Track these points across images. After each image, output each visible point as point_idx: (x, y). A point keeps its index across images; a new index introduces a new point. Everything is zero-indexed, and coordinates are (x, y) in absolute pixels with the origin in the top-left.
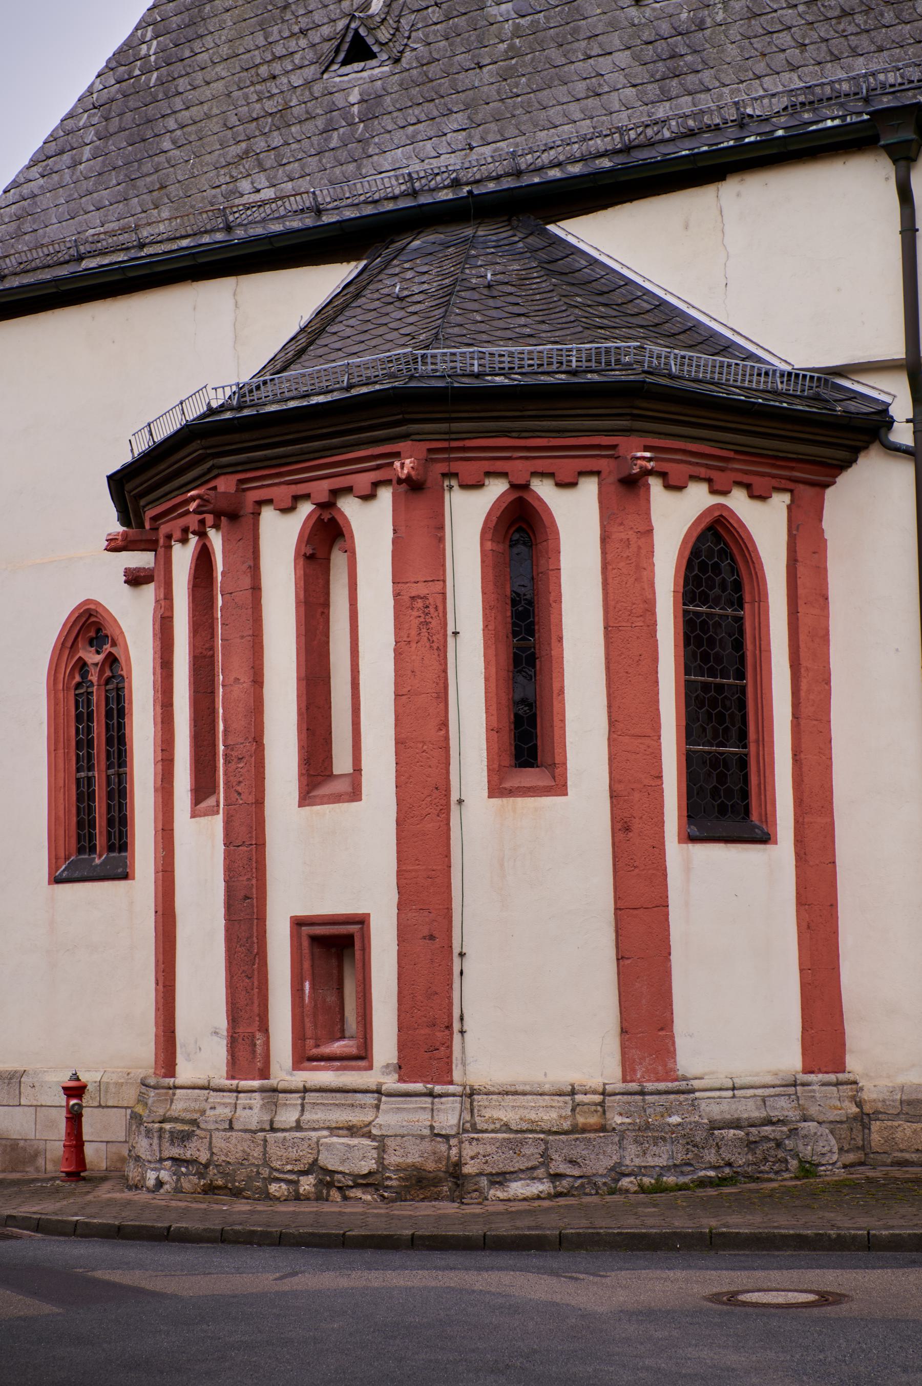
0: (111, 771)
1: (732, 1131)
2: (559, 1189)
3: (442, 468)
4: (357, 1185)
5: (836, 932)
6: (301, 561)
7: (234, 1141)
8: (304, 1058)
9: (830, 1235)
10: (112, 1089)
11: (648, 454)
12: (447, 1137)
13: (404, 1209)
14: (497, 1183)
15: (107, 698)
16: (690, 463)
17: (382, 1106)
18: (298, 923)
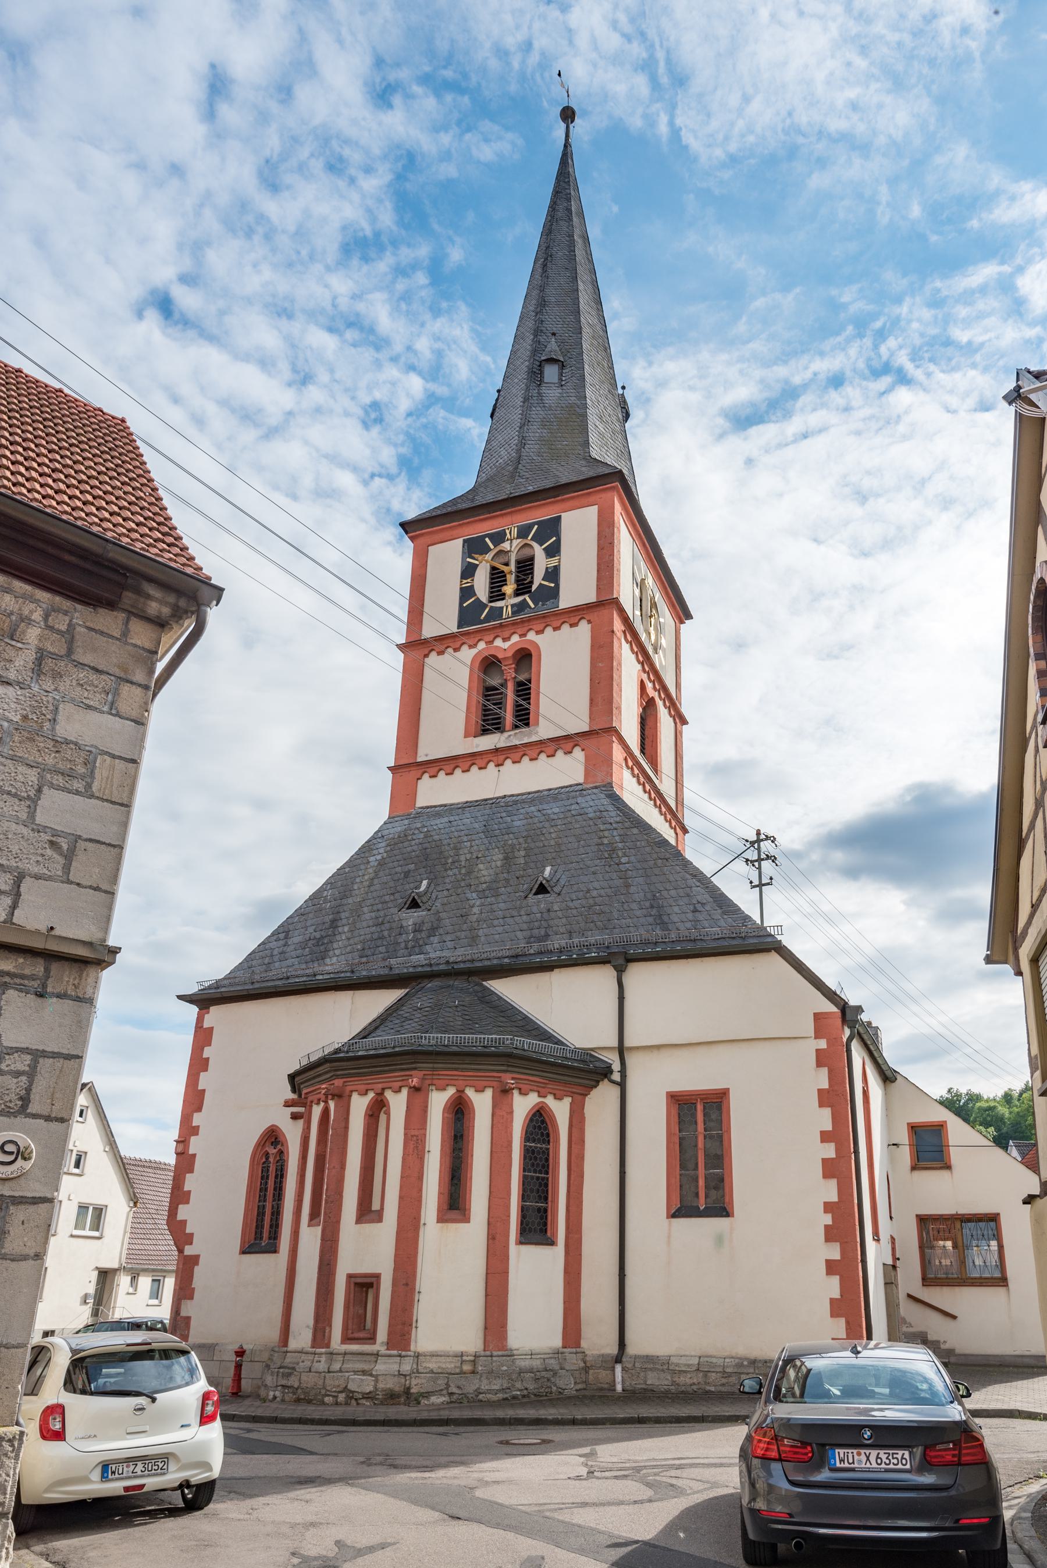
2: (67, 786)
3: (428, 1082)
4: (363, 1398)
8: (346, 1339)
12: (405, 1376)
13: (382, 1409)
18: (350, 1276)
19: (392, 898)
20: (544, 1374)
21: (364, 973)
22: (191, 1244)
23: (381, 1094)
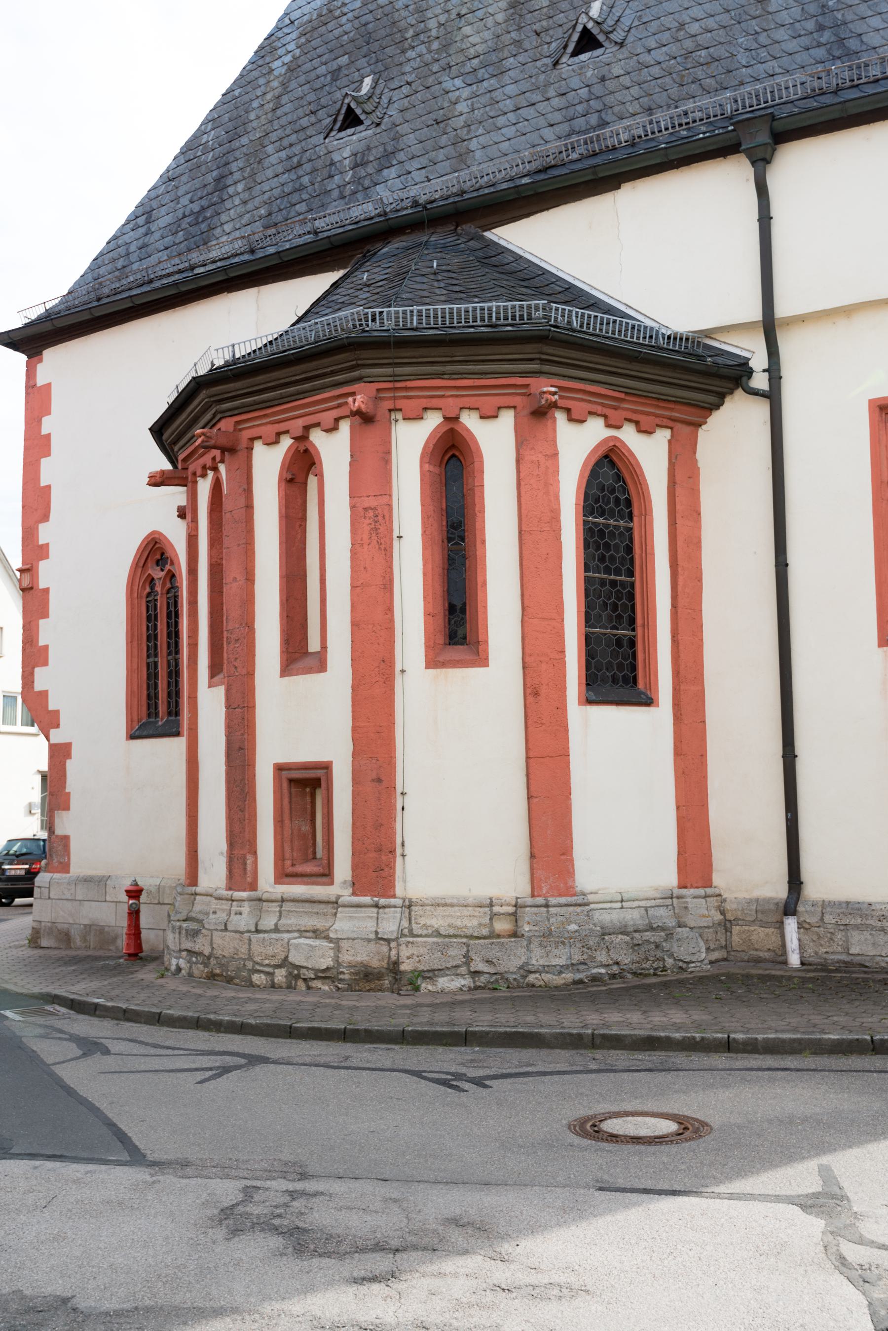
0: (170, 658)
1: (620, 936)
2: (478, 984)
3: (389, 404)
4: (317, 978)
5: (705, 777)
6: (283, 484)
7: (227, 939)
8: (283, 875)
9: (694, 1038)
10: (168, 891)
11: (553, 389)
12: (388, 941)
13: (350, 1000)
14: (429, 978)
15: (168, 604)
16: (590, 402)
17: (339, 915)
18: (279, 769)
19: (313, 119)
20: (648, 935)
21: (272, 250)
22: (57, 726)
23: (302, 438)
